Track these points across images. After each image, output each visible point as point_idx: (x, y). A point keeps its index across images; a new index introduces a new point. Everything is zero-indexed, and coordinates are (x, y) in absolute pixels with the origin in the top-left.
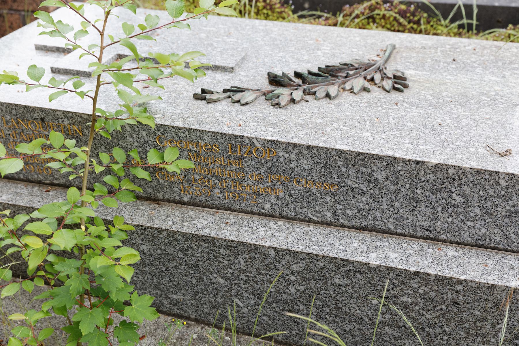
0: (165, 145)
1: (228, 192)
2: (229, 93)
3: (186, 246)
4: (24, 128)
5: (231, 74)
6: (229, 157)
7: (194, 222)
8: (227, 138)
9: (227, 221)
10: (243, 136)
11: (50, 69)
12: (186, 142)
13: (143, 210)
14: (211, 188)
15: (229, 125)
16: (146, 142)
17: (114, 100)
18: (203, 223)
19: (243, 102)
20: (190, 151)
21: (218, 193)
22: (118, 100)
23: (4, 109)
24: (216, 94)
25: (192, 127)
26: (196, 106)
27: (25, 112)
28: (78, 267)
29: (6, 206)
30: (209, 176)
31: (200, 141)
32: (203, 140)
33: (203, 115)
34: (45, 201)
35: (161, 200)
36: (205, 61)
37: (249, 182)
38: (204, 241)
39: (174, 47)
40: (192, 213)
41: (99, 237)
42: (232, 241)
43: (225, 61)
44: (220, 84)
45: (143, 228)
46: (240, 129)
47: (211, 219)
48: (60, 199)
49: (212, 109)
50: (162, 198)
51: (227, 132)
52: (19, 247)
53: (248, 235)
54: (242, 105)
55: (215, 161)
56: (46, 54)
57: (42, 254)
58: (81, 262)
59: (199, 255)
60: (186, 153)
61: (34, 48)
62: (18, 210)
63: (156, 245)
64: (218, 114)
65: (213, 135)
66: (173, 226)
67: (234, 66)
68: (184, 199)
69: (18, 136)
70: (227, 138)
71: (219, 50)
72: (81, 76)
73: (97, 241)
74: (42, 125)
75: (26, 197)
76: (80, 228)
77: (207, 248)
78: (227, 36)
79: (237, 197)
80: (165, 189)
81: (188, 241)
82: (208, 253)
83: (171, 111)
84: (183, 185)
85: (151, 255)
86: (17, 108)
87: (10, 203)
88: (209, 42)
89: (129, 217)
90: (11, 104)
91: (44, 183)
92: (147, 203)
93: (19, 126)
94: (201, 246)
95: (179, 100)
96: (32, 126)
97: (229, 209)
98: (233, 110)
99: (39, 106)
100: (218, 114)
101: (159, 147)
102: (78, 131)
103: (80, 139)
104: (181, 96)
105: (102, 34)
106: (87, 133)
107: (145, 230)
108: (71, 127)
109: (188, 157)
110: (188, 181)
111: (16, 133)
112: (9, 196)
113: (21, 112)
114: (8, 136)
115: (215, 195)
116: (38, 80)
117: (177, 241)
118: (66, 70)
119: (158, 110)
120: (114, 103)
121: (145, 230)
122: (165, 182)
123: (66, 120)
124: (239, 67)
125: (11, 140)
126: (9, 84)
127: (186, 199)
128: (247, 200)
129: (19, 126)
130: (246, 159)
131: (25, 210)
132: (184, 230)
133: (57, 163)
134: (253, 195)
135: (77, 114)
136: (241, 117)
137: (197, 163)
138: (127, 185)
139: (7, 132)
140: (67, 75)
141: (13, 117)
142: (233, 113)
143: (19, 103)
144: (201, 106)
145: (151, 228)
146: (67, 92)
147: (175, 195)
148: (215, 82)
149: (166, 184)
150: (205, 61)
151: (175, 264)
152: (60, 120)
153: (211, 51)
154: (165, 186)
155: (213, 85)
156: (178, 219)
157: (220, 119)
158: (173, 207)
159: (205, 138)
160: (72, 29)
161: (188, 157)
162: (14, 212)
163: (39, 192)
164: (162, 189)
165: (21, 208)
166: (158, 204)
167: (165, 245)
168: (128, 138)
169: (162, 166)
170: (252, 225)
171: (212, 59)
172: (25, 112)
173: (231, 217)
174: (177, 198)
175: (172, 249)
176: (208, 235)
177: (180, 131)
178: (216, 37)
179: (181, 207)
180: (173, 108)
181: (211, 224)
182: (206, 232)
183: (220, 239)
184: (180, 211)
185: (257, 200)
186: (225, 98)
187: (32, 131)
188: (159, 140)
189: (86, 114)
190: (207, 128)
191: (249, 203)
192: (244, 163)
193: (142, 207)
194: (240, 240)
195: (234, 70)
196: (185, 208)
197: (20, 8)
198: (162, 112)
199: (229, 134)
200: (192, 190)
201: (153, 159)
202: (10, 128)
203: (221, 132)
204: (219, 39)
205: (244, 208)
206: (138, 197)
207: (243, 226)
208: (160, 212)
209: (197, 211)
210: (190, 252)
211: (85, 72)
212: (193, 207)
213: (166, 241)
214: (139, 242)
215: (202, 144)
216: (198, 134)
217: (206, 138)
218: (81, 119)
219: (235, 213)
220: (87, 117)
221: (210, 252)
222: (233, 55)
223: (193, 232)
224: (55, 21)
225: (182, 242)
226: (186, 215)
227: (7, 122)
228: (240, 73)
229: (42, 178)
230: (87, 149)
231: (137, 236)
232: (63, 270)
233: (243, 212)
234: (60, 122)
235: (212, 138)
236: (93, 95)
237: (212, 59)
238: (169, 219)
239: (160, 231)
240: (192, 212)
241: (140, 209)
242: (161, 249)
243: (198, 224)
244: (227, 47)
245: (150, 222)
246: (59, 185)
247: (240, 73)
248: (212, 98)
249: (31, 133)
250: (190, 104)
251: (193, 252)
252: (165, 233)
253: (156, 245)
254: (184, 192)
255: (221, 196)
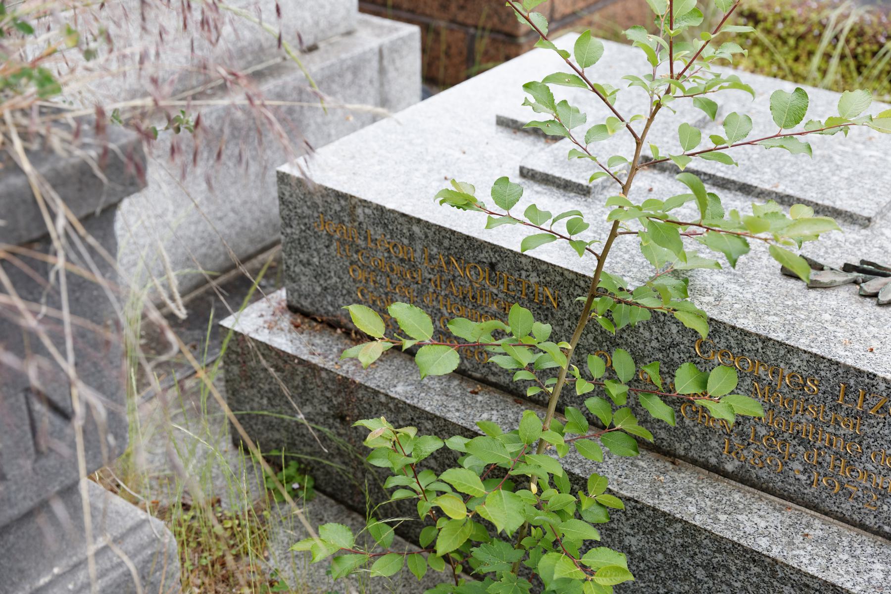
0: (711, 358)
1: (819, 474)
2: (855, 274)
3: (715, 561)
4: (457, 274)
5: (863, 232)
6: (836, 408)
7: (740, 517)
8: (840, 371)
9: (807, 531)
10: (875, 375)
11: (518, 168)
12: (753, 362)
13: (642, 469)
14: (786, 459)
15: (849, 346)
16: (674, 345)
17: (627, 251)
18: (759, 525)
19: (882, 298)
20: (759, 379)
21: (799, 471)
22: (634, 252)
23: (430, 234)
24: (829, 271)
25: (772, 335)
26: (783, 291)
27: (465, 247)
28: (514, 561)
29: (400, 405)
30: (786, 435)
31: (782, 365)
32: (789, 364)
33: (798, 313)
34: (468, 411)
35: (680, 457)
36: (815, 195)
37: (869, 466)
38: (754, 561)
39: (755, 156)
40: (737, 496)
41: (560, 513)
42: (812, 577)
43: (854, 202)
44: (837, 250)
45: (639, 506)
46: (870, 359)
47: (775, 518)
48: (494, 412)
49: (816, 303)
50: (683, 453)
51: (842, 361)
52: (415, 491)
53: (847, 572)
54: (880, 305)
55: (805, 410)
56: (514, 136)
57: (463, 531)
58: (520, 554)
59: (738, 585)
60: (749, 381)
61: (494, 120)
62: (419, 418)
63: (656, 543)
64: (826, 317)
65: (813, 359)
66: (697, 517)
67: (872, 215)
68: (726, 467)
69: (444, 286)
70: (840, 371)
71: (845, 173)
72: (572, 191)
73: (554, 520)
74: (490, 275)
75: (437, 397)
76: (530, 489)
77: (758, 575)
78: (864, 143)
79: (837, 489)
80: (693, 438)
81: (721, 553)
82: (758, 587)
83: (733, 292)
84: (729, 440)
85: (643, 559)
86: (453, 237)
87: (408, 402)
88: (826, 152)
89: (616, 477)
90: (444, 229)
91: (470, 376)
92: (652, 456)
93: (450, 268)
94: (746, 570)
95: (752, 272)
96: (473, 273)
97: (816, 508)
98: (861, 312)
99: (491, 241)
100: (826, 317)
101: (698, 360)
102: (551, 298)
103: (552, 314)
104: (756, 263)
105: (639, 143)
106: (567, 305)
107: (641, 510)
108: (541, 289)
109: (753, 390)
110: (741, 434)
111: (441, 280)
112: (409, 388)
113: (458, 245)
114: (427, 281)
115: (791, 473)
116: (508, 208)
117: (699, 546)
118: (547, 175)
119: (709, 287)
120: (627, 256)
121: (641, 510)
122: (694, 426)
123: (535, 274)
124: (882, 218)
125: (431, 290)
126: (459, 208)
127: (729, 467)
128: (856, 499)
129: (450, 268)
130: (872, 421)
131: (432, 420)
132: (718, 530)
133: (509, 358)
134: (871, 493)
135: (557, 269)
136: (874, 330)
137: (768, 406)
138: (626, 423)
139: (427, 275)
140: (546, 184)
141: (442, 252)
142: (859, 320)
143: (459, 230)
144: (794, 291)
145: (654, 509)
146: (556, 238)
147: (710, 453)
148: (829, 243)
149: (696, 429)
150: (815, 195)
151: (687, 588)
152: (524, 274)
153: (829, 175)
154: (694, 433)
155: (823, 250)
156: (709, 503)
157: (831, 328)
158: (702, 476)
159: (794, 361)
160: (584, 120)
161: (753, 390)
162: (412, 419)
163: (459, 392)
164: (687, 437)
165: (425, 415)
166: (673, 463)
167: (674, 547)
168: (641, 330)
169: (699, 402)
170: (858, 552)
171: (829, 193)
172: (465, 247)
173: (817, 523)
174: (713, 461)
175: (687, 560)
176: (765, 553)
177: (746, 338)
178: (841, 144)
179: (717, 480)
180: (738, 288)
181: (772, 530)
182: (762, 544)
183: (787, 566)
184: (715, 487)
185: (879, 503)
186: (846, 283)
187: (471, 282)
188: (701, 346)
189: (572, 272)
190: (802, 343)
191: (861, 505)
192: (865, 428)
193: (641, 463)
194: (830, 579)
195: (872, 224)
196: (724, 485)
197: (470, 21)
198: (715, 292)
199: (845, 365)
200: (745, 452)
201: (685, 381)
202: (432, 269)
203: (829, 357)
204: (847, 149)
205: (847, 514)
206: (641, 444)
207: (840, 550)
208: (674, 481)
209: (748, 496)
210: (720, 574)
211: (579, 185)
212: (740, 485)
213: (677, 540)
214: (625, 529)
215: (786, 372)
216: (782, 352)
217: (796, 361)
218: (561, 279)
219: (827, 518)
220: (574, 277)
221: (762, 584)
222: (872, 191)
223: (735, 539)
224: (557, 101)
225: (709, 552)
226: (725, 499)
227: (431, 258)
228: (884, 230)
229: (468, 366)
230: (570, 347)
231: (623, 518)
232: (487, 561)
233: (843, 519)
234: (523, 276)
235: (809, 366)
236: (599, 252)
237: (829, 193)
238: (690, 499)
239: (670, 519)
240: (738, 496)
241: (637, 466)
242: (664, 553)
243: (748, 524)
244: (861, 168)
245: (653, 498)
246: (496, 386)
247: (884, 230)
248: (818, 279)
249: (468, 284)
250: (771, 285)
251: (728, 576)
252: (679, 526)
253: (656, 543)
254: (730, 453)
255: (803, 478)
